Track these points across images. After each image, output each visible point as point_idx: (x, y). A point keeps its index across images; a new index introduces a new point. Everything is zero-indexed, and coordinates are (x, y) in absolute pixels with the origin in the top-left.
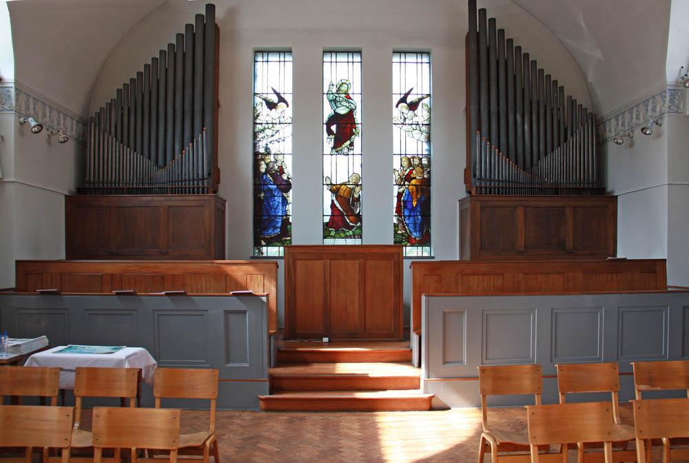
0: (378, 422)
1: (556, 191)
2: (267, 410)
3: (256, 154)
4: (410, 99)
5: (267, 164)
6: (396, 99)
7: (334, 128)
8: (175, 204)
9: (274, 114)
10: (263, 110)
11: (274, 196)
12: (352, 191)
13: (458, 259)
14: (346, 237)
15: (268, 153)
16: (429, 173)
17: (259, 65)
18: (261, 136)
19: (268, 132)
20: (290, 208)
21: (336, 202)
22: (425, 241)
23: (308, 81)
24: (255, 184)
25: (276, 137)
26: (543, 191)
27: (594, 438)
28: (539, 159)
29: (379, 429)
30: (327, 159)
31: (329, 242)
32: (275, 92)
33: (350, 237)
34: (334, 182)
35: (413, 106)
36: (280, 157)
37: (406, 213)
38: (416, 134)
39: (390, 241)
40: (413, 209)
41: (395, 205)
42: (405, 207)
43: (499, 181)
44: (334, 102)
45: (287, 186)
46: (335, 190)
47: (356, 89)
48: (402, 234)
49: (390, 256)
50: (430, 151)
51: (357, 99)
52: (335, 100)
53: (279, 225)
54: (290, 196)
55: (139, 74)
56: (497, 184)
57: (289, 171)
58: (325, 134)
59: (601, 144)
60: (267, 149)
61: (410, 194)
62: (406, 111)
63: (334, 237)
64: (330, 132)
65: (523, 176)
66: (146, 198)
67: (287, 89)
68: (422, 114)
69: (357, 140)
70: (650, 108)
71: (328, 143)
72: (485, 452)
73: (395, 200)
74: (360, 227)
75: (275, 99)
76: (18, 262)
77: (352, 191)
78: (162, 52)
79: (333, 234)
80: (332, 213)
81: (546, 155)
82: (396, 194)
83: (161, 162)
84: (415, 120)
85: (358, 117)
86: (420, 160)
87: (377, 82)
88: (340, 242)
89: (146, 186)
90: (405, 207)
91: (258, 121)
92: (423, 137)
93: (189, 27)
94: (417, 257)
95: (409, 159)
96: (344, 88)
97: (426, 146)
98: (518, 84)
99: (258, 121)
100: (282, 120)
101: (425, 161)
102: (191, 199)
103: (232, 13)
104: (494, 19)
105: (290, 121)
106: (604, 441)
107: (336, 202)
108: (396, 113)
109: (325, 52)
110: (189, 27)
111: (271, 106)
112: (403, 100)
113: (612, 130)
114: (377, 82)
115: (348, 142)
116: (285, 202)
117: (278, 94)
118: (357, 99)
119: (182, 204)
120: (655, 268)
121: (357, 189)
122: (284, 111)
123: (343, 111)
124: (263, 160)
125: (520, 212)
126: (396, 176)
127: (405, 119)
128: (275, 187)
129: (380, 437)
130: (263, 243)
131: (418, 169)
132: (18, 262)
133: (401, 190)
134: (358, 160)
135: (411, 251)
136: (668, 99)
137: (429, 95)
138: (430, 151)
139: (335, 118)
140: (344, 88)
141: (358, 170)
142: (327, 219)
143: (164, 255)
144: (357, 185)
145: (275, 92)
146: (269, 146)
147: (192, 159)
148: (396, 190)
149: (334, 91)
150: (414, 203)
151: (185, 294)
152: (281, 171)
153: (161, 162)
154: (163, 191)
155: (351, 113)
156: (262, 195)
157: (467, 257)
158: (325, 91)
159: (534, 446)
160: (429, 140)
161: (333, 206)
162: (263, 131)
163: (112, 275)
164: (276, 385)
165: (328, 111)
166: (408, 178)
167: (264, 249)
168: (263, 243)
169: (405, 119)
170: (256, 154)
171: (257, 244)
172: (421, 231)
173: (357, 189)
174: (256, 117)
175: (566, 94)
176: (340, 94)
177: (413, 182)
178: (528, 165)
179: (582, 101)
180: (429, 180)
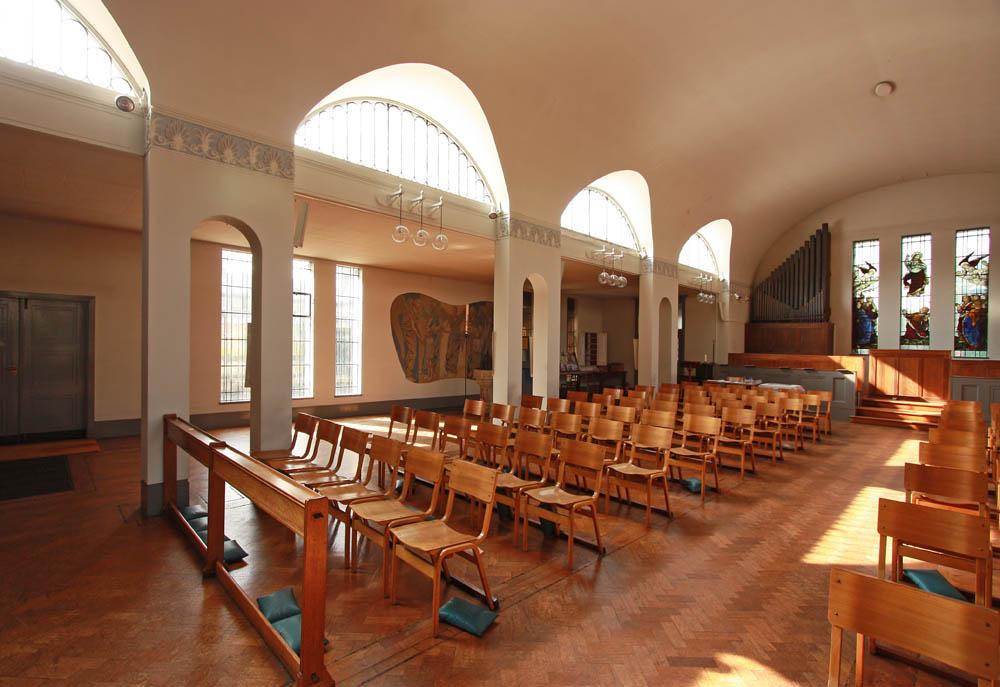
4: (970, 260)
6: (958, 260)
7: (909, 281)
10: (860, 274)
12: (922, 318)
15: (862, 297)
16: (987, 305)
19: (863, 286)
21: (911, 325)
22: (983, 346)
35: (974, 264)
44: (909, 266)
45: (875, 315)
46: (910, 317)
58: (903, 286)
61: (969, 318)
64: (906, 284)
66: (787, 325)
67: (876, 262)
68: (981, 267)
71: (905, 290)
73: (957, 323)
74: (928, 339)
75: (867, 267)
76: (730, 355)
83: (796, 306)
85: (928, 273)
87: (944, 253)
90: (966, 326)
97: (984, 288)
103: (839, 223)
108: (959, 269)
111: (865, 271)
114: (944, 253)
116: (874, 324)
123: (916, 270)
139: (910, 276)
141: (928, 306)
142: (903, 334)
143: (798, 352)
148: (958, 316)
149: (910, 259)
150: (973, 324)
152: (871, 307)
153: (796, 306)
155: (923, 272)
160: (987, 284)
161: (908, 326)
164: (859, 412)
165: (905, 271)
166: (969, 308)
171: (854, 347)
176: (916, 259)
177: (973, 311)
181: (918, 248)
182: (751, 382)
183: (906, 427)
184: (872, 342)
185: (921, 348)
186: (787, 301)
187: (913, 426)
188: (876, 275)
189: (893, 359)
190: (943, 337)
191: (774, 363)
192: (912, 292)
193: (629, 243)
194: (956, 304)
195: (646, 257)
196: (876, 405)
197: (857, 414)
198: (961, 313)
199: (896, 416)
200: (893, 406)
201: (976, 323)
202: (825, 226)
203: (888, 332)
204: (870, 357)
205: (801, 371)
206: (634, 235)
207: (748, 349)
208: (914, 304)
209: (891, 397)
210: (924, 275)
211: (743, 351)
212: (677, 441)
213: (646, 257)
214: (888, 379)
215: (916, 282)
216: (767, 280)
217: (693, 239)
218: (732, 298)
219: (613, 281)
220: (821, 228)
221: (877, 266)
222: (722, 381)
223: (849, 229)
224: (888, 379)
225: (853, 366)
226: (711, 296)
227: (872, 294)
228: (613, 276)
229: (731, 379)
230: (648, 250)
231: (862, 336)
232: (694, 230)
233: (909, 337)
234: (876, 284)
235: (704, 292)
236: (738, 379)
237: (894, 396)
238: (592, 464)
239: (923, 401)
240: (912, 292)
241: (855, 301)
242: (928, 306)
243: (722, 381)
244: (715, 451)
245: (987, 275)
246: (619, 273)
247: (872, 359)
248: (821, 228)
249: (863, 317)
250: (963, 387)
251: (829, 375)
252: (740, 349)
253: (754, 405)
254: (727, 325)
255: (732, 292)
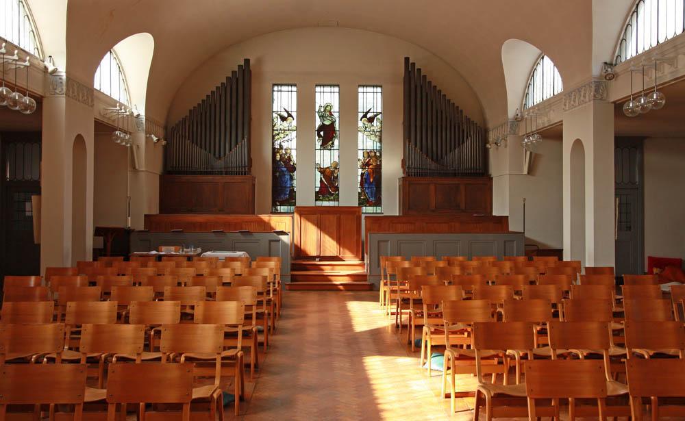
0: (373, 384)
1: (455, 175)
2: (290, 290)
3: (274, 149)
4: (369, 115)
5: (281, 155)
6: (361, 115)
7: (322, 133)
8: (228, 181)
9: (285, 124)
10: (278, 122)
11: (285, 175)
12: (333, 172)
13: (398, 214)
14: (329, 200)
15: (281, 147)
16: (381, 161)
17: (275, 93)
18: (276, 137)
19: (282, 135)
20: (295, 182)
21: (323, 179)
22: (378, 203)
23: (306, 103)
24: (273, 168)
25: (286, 138)
26: (446, 175)
27: (588, 393)
28: (446, 154)
29: (374, 390)
30: (318, 152)
31: (319, 203)
32: (286, 111)
33: (332, 201)
34: (322, 167)
35: (371, 120)
36: (289, 151)
37: (367, 186)
38: (373, 137)
39: (357, 205)
40: (371, 183)
41: (359, 181)
42: (366, 182)
43: (415, 168)
44: (322, 117)
45: (293, 169)
46: (323, 171)
47: (336, 108)
48: (364, 199)
49: (353, 212)
50: (381, 147)
51: (336, 115)
52: (323, 116)
53: (288, 193)
54: (295, 174)
55: (203, 101)
56: (413, 170)
57: (294, 159)
58: (317, 138)
59: (485, 141)
60: (280, 145)
61: (369, 174)
62: (366, 123)
63: (322, 200)
64: (319, 136)
65: (433, 166)
66: (210, 178)
67: (293, 108)
69: (336, 142)
70: (582, 94)
71: (318, 144)
72: (492, 417)
73: (359, 178)
74: (338, 195)
75: (285, 115)
76: (145, 215)
77: (333, 172)
78: (217, 88)
79: (321, 198)
80: (321, 185)
81: (455, 148)
82: (360, 174)
83: (217, 156)
84: (372, 128)
85: (337, 126)
86: (375, 153)
87: (349, 103)
88: (325, 204)
89: (209, 170)
90: (366, 182)
91: (275, 129)
92: (377, 139)
93: (234, 72)
94: (373, 213)
95: (368, 153)
96: (328, 108)
97: (378, 144)
98: (434, 109)
99: (275, 129)
100: (290, 128)
101: (378, 154)
102: (238, 178)
103: (259, 61)
104: (420, 69)
105: (295, 128)
106: (598, 397)
107: (323, 179)
108: (360, 124)
109: (317, 86)
110: (234, 72)
111: (283, 119)
112: (365, 116)
113: (492, 136)
114: (349, 103)
115: (331, 142)
116: (292, 178)
117: (287, 112)
118: (336, 115)
119: (233, 181)
120: (503, 221)
121: (336, 171)
122: (291, 122)
123: (327, 123)
124: (278, 152)
125: (432, 187)
126: (360, 163)
127: (366, 128)
128: (285, 169)
129: (370, 376)
130: (278, 204)
131: (373, 158)
132: (145, 215)
133: (363, 172)
134: (336, 153)
135: (368, 210)
136: (509, 126)
137: (381, 113)
138: (381, 147)
139: (322, 127)
140: (328, 108)
141: (337, 159)
142: (317, 189)
143: (221, 211)
144: (336, 169)
145: (286, 111)
146: (282, 144)
147: (236, 155)
148: (360, 171)
149: (322, 110)
150: (371, 180)
151: (248, 232)
152: (290, 159)
153: (217, 156)
154: (220, 173)
155: (333, 124)
156: (278, 174)
157: (401, 214)
158: (317, 110)
159: (531, 399)
160: (380, 141)
161: (321, 181)
162: (278, 134)
163: (201, 223)
164: (294, 278)
165: (318, 123)
167: (279, 207)
168: (278, 204)
169: (366, 128)
170: (274, 149)
171: (274, 205)
172: (375, 197)
173: (336, 171)
174: (273, 126)
175: (464, 114)
176: (326, 112)
177: (371, 167)
178: (437, 159)
179: (475, 118)
180: (381, 165)
181: (327, 97)
182: (191, 251)
183: (334, 288)
184: (290, 199)
185: (332, 204)
186: (208, 149)
187: (341, 287)
188: (294, 123)
189: (314, 217)
190: (349, 195)
191: (203, 226)
192: (324, 146)
193: (28, 44)
194: (359, 160)
195: (55, 71)
196: (305, 268)
197: (292, 280)
198: (363, 169)
199: (326, 278)
200: (318, 267)
201: (374, 179)
202: (247, 61)
203: (306, 186)
204: (295, 214)
205: (235, 235)
206: (35, 33)
207: (164, 208)
208: (326, 158)
209: (314, 258)
210: (334, 128)
211: (158, 212)
212: (230, 343)
213: (55, 71)
214: (313, 240)
215: (328, 134)
216: (184, 119)
217: (106, 61)
218: (148, 139)
219: (15, 103)
220: (242, 63)
221: (294, 114)
222: (154, 252)
223: (270, 68)
224: (313, 240)
225: (282, 222)
226: (128, 137)
227: (290, 144)
228: (16, 95)
229: (164, 248)
230: (58, 63)
231: (282, 195)
232: (108, 48)
233: (323, 193)
234: (294, 134)
235: (121, 130)
236: (173, 248)
237: (317, 257)
238: (172, 397)
239: (341, 260)
240: (324, 146)
241: (275, 152)
242: (337, 159)
243: (154, 252)
244: (239, 345)
245: (381, 132)
246: (23, 92)
247: (296, 216)
248: (242, 63)
249: (283, 168)
250: (379, 242)
251: (264, 237)
252: (155, 211)
253: (144, 280)
254: (143, 176)
255: (148, 132)
